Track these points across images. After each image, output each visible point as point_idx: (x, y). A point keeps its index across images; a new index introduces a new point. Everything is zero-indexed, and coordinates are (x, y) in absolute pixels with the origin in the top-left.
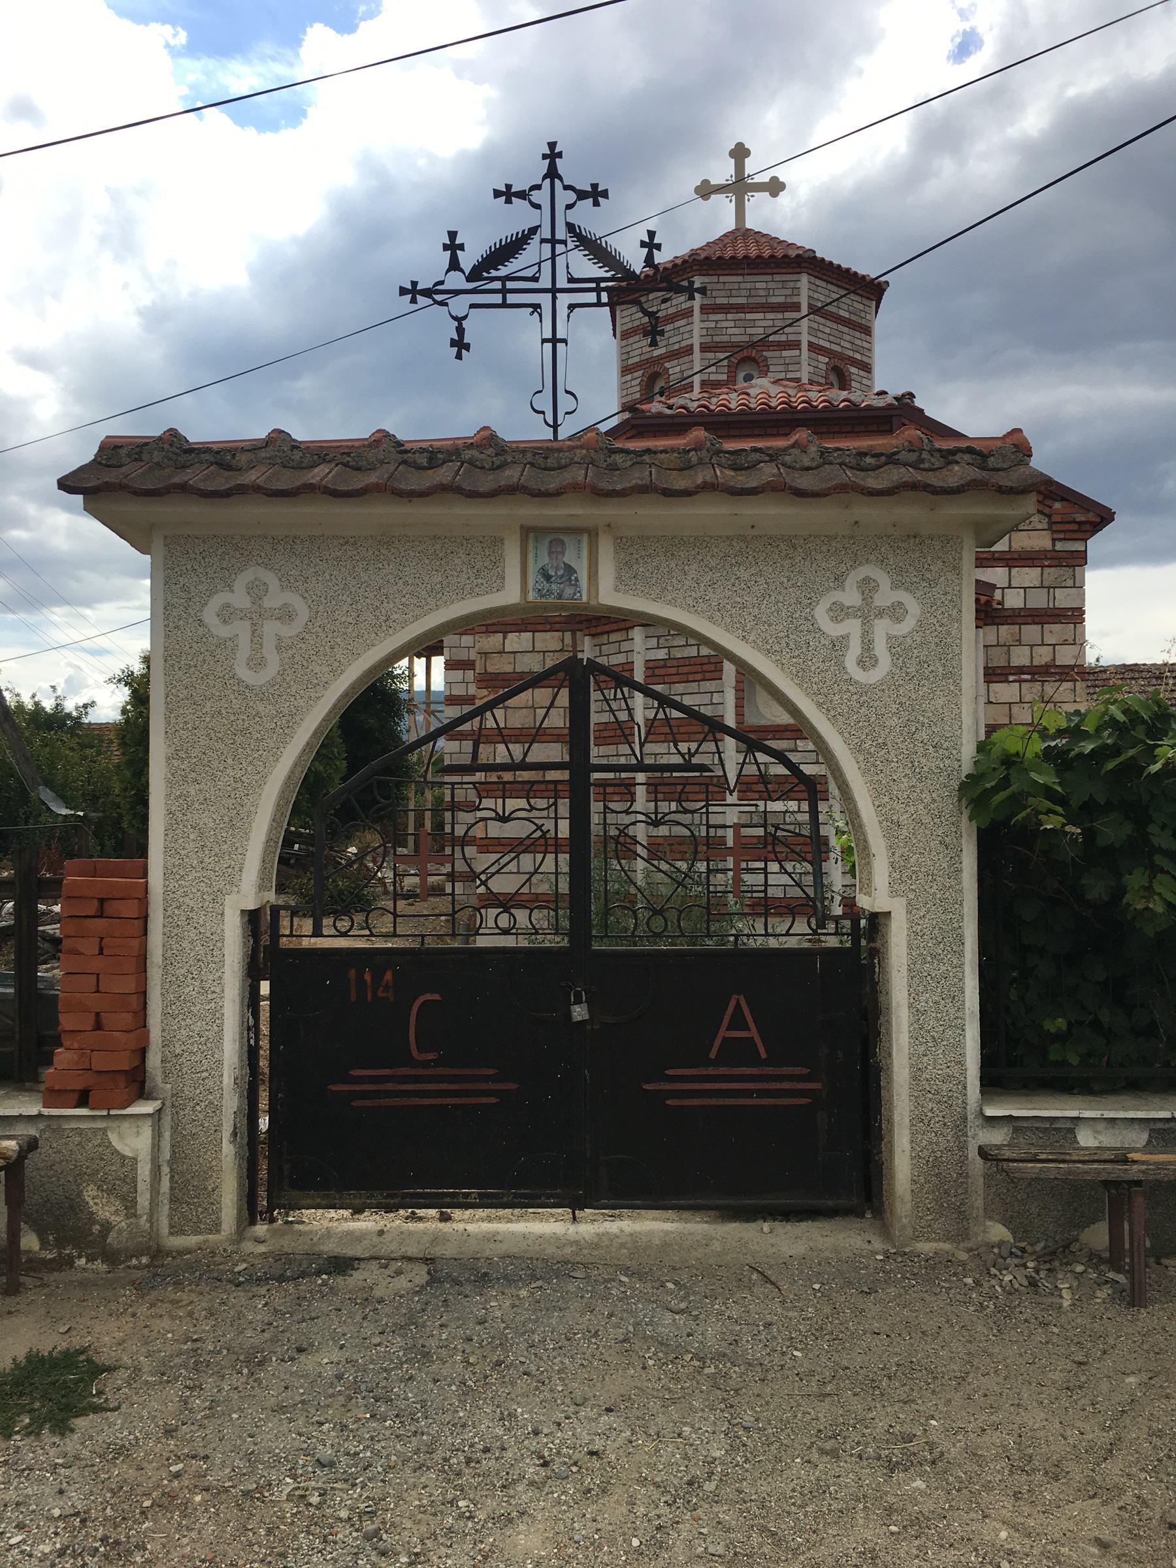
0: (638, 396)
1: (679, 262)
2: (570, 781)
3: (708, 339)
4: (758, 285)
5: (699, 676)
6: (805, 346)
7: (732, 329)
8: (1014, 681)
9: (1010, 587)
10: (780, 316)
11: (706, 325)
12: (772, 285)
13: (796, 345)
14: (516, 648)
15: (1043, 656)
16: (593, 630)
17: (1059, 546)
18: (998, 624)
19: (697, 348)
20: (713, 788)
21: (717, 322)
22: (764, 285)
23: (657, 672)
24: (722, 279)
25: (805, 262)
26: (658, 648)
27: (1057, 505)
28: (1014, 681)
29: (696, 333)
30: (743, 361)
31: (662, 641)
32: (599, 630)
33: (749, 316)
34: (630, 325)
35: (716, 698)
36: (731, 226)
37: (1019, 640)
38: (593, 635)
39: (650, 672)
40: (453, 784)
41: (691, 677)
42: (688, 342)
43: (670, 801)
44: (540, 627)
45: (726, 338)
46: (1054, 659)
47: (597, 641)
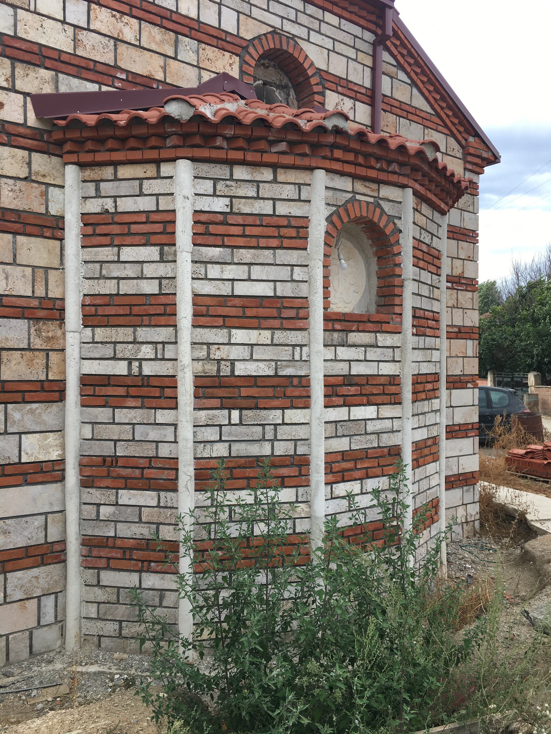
2: (241, 409)
5: (274, 243)
16: (87, 158)
23: (212, 229)
26: (214, 195)
27: (471, 139)
31: (220, 186)
32: (100, 157)
35: (298, 273)
38: (82, 165)
39: (201, 229)
40: (60, 431)
41: (263, 242)
43: (230, 409)
47: (89, 173)
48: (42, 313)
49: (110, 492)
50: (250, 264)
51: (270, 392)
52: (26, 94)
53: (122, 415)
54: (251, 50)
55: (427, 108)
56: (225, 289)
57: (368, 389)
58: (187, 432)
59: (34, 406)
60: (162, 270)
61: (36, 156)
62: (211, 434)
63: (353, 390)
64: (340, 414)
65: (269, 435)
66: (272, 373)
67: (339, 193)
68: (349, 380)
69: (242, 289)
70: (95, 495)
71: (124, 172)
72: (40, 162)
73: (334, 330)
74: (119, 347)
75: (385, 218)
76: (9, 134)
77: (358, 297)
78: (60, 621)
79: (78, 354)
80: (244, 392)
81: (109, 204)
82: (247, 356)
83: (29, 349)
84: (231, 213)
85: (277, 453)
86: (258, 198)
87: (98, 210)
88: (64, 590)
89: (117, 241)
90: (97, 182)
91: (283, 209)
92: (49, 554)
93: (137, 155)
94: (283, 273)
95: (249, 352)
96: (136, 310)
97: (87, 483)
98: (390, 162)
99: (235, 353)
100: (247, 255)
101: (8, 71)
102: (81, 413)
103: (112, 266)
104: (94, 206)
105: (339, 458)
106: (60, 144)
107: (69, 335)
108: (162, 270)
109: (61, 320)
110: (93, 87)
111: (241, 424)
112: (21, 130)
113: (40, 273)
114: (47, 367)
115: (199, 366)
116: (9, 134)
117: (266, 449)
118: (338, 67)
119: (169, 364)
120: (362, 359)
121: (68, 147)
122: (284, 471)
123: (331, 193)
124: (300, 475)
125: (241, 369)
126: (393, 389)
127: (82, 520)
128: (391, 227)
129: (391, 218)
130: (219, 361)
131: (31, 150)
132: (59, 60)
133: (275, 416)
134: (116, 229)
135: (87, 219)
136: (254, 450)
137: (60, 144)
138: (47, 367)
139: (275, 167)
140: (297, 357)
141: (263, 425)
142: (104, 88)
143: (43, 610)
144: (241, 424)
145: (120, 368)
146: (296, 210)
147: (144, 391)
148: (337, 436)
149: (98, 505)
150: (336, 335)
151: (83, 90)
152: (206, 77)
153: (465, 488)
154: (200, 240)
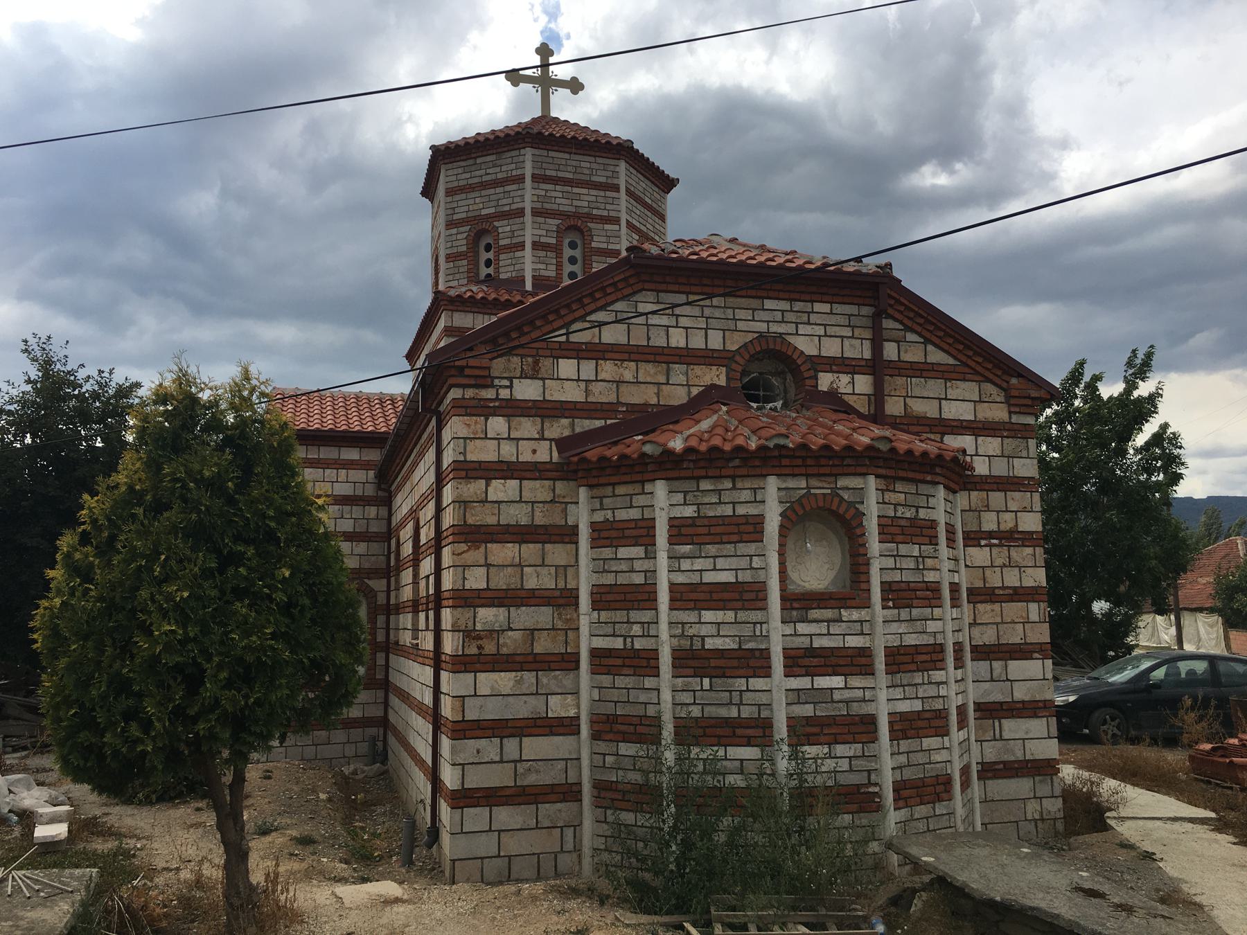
0: (464, 248)
1: (482, 139)
2: (711, 677)
3: (539, 205)
4: (583, 164)
5: (735, 538)
6: (623, 223)
7: (560, 199)
8: (986, 546)
9: (977, 455)
10: (602, 193)
11: (537, 192)
12: (594, 166)
13: (616, 221)
14: (501, 496)
15: (1008, 521)
16: (594, 481)
17: (1015, 419)
18: (969, 490)
19: (528, 212)
20: (753, 662)
21: (547, 191)
22: (588, 165)
23: (683, 531)
24: (552, 154)
25: (622, 150)
26: (685, 504)
27: (1014, 381)
28: (986, 546)
29: (528, 198)
30: (569, 228)
32: (602, 480)
33: (576, 190)
34: (456, 184)
35: (757, 562)
36: (538, 114)
37: (987, 506)
38: (591, 486)
39: (675, 531)
40: (576, 693)
41: (725, 538)
42: (520, 205)
44: (528, 475)
45: (555, 207)
46: (1017, 525)
47: (596, 492)
48: (562, 601)
49: (611, 744)
50: (715, 557)
51: (735, 663)
52: (551, 440)
53: (621, 681)
54: (738, 358)
55: (951, 361)
56: (695, 579)
57: (833, 660)
58: (666, 694)
59: (558, 673)
60: (646, 565)
61: (559, 484)
62: (686, 698)
63: (815, 661)
64: (803, 683)
65: (736, 700)
66: (736, 647)
67: (792, 492)
68: (811, 652)
69: (709, 577)
70: (602, 747)
71: (620, 490)
72: (560, 486)
73: (793, 609)
74: (617, 626)
75: (844, 506)
76: (540, 471)
77: (831, 575)
78: (577, 849)
79: (589, 634)
80: (713, 663)
81: (609, 514)
82: (714, 632)
83: (553, 629)
84: (699, 517)
85: (743, 716)
86: (720, 503)
87: (602, 519)
88: (580, 824)
89: (615, 543)
90: (601, 498)
91: (741, 510)
92: (570, 793)
93: (627, 478)
94: (744, 563)
95: (717, 629)
96: (628, 596)
97: (596, 736)
98: (843, 458)
99: (704, 630)
100: (712, 549)
101: (539, 426)
102: (591, 680)
103: (612, 562)
104: (599, 517)
105: (804, 723)
106: (576, 471)
107: (582, 617)
108: (646, 565)
109: (577, 605)
110: (599, 423)
111: (711, 690)
112: (548, 466)
113: (561, 570)
114: (566, 642)
115: (675, 641)
116: (540, 471)
117: (734, 713)
118: (831, 349)
119: (653, 640)
120: (817, 632)
121: (580, 474)
122: (750, 732)
123: (783, 493)
124: (764, 736)
125: (710, 644)
126: (863, 661)
127: (593, 767)
128: (852, 511)
129: (851, 504)
130: (691, 637)
131: (554, 480)
132: (575, 409)
133: (740, 683)
134: (614, 534)
135: (594, 526)
136: (723, 712)
137: (576, 471)
138: (566, 642)
139: (733, 478)
140: (758, 633)
141: (730, 691)
142: (609, 422)
143: (565, 839)
144: (711, 690)
145: (618, 643)
146: (752, 510)
147: (635, 662)
148: (799, 703)
149: (604, 755)
150: (795, 613)
151: (592, 427)
152: (695, 391)
153: (1037, 778)
154: (674, 540)
